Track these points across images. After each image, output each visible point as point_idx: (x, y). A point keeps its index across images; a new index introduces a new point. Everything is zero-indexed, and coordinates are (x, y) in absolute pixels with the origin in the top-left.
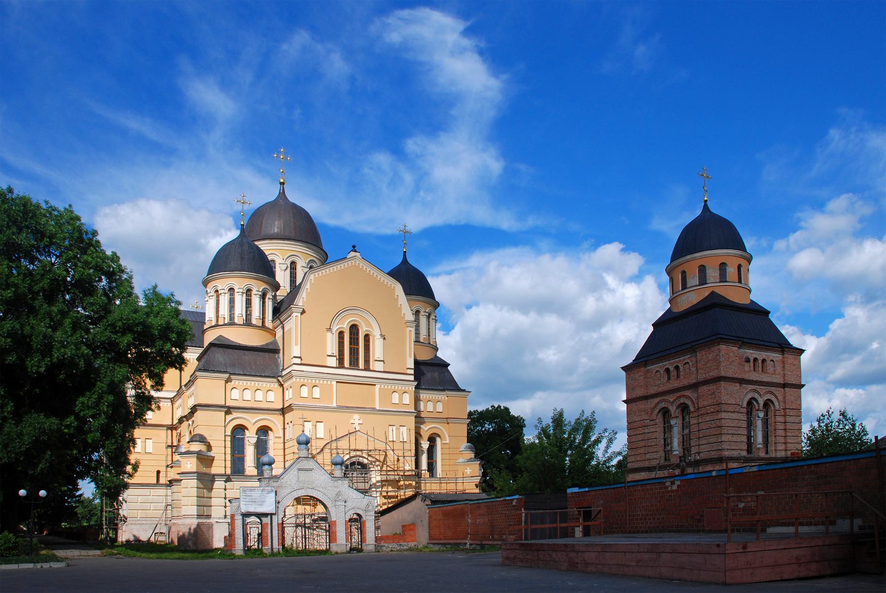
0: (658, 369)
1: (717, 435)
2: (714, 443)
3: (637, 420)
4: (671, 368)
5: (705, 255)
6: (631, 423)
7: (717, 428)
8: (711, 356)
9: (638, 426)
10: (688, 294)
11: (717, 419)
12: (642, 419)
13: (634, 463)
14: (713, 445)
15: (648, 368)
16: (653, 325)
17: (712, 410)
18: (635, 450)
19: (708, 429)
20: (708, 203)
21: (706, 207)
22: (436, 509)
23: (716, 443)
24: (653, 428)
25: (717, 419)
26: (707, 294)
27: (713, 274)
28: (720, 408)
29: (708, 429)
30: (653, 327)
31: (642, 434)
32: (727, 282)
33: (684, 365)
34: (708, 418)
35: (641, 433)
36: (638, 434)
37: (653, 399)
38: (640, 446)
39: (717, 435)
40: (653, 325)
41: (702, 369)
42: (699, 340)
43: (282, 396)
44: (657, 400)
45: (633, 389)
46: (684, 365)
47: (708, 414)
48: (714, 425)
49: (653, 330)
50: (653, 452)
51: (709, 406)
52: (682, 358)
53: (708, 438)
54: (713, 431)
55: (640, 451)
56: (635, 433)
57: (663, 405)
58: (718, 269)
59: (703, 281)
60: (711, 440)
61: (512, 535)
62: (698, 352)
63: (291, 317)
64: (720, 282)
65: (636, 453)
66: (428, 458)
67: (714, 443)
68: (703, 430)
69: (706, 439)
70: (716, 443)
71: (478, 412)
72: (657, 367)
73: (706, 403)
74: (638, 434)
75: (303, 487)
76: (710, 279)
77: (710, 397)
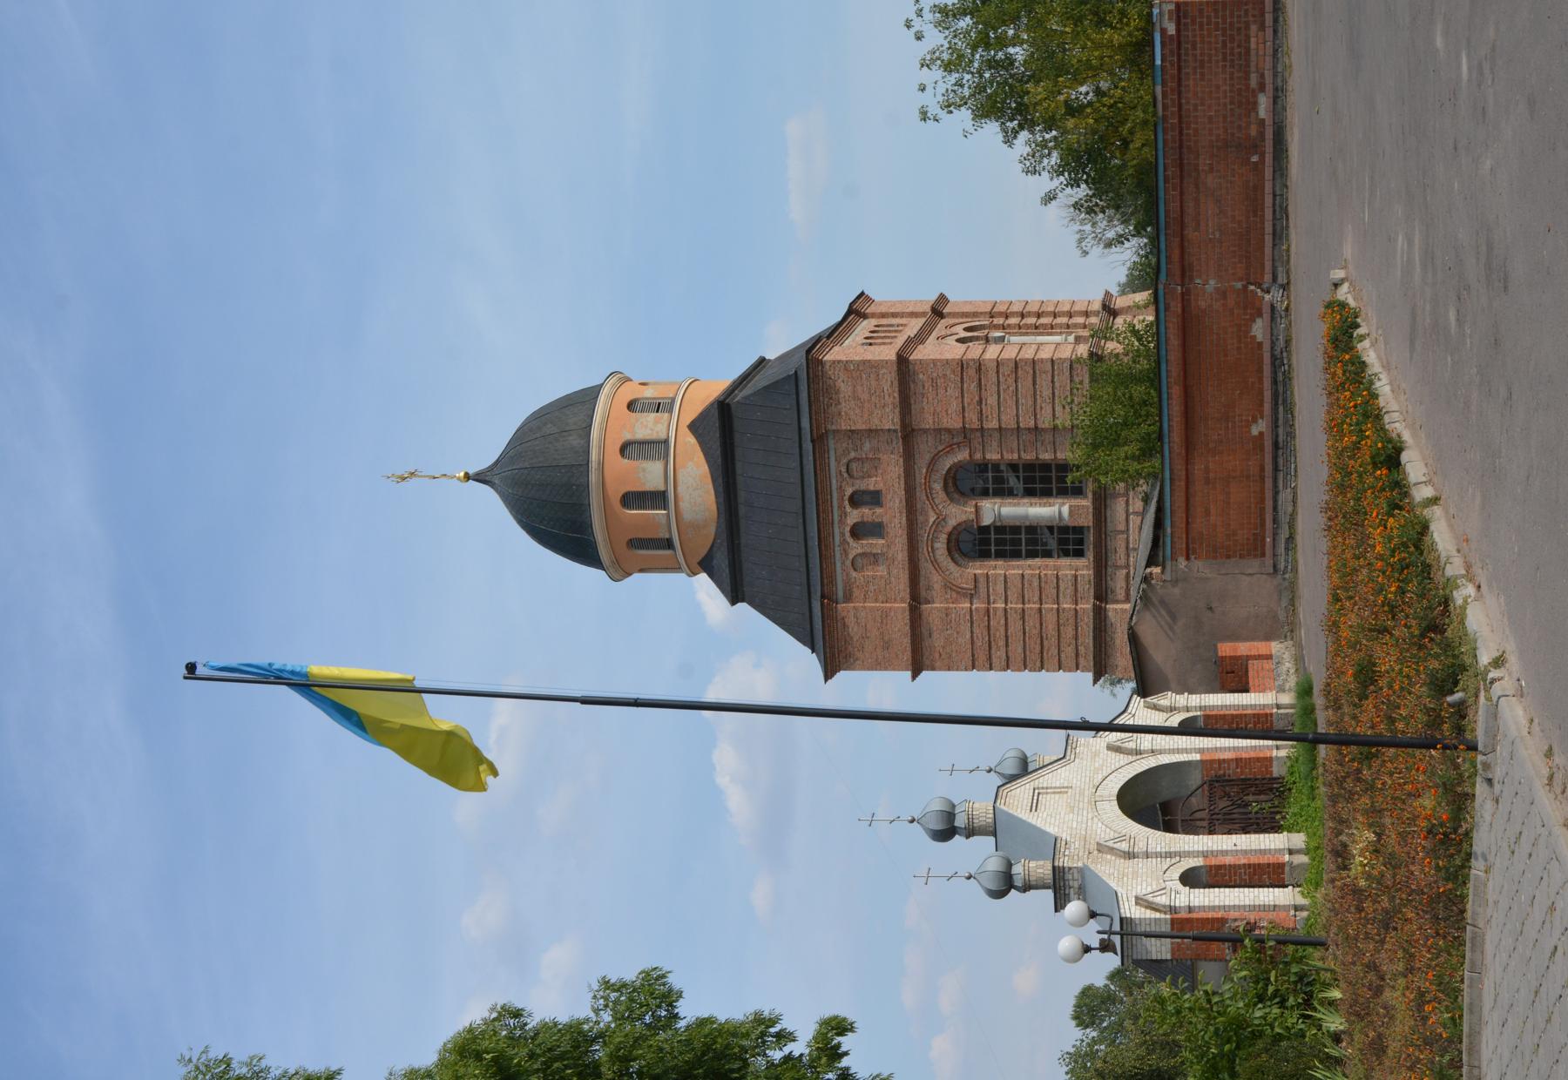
0: (848, 563)
1: (1034, 372)
2: (1053, 382)
3: (968, 636)
4: (854, 516)
5: (600, 447)
6: (973, 655)
7: (1020, 372)
8: (844, 387)
9: (986, 633)
10: (680, 489)
11: (998, 372)
12: (968, 617)
13: (1081, 649)
14: (1057, 385)
15: (840, 594)
16: (733, 603)
17: (974, 385)
18: (1045, 643)
19: (1017, 402)
20: (472, 471)
21: (481, 478)
22: (794, 477)
23: (1053, 376)
24: (995, 584)
25: (998, 372)
26: (692, 440)
27: (648, 426)
28: (971, 363)
29: (1017, 402)
30: (739, 604)
31: (1006, 619)
32: (673, 400)
33: (851, 476)
34: (992, 400)
35: (1003, 622)
36: (1006, 630)
37: (922, 579)
38: (1038, 625)
39: (1034, 372)
40: (733, 603)
41: (871, 413)
42: (800, 429)
43: (1117, 714)
44: (926, 566)
45: (887, 645)
46: (851, 476)
47: (981, 400)
48: (1011, 381)
49: (745, 604)
50: (1058, 587)
51: (963, 397)
52: (834, 481)
53: (1039, 401)
54: (1025, 384)
55: (1050, 627)
56: (1002, 643)
57: (941, 546)
58: (638, 415)
59: (656, 448)
60: (1047, 393)
61: (1248, 37)
62: (829, 427)
63: (1119, 895)
64: (671, 411)
65: (1054, 641)
66: (1064, 494)
67: (1053, 382)
68: (1017, 415)
69: (1041, 408)
70: (1053, 376)
71: (1272, 775)
72: (843, 563)
73: (955, 406)
74: (1006, 630)
75: (1090, 802)
76: (657, 432)
77: (941, 391)
